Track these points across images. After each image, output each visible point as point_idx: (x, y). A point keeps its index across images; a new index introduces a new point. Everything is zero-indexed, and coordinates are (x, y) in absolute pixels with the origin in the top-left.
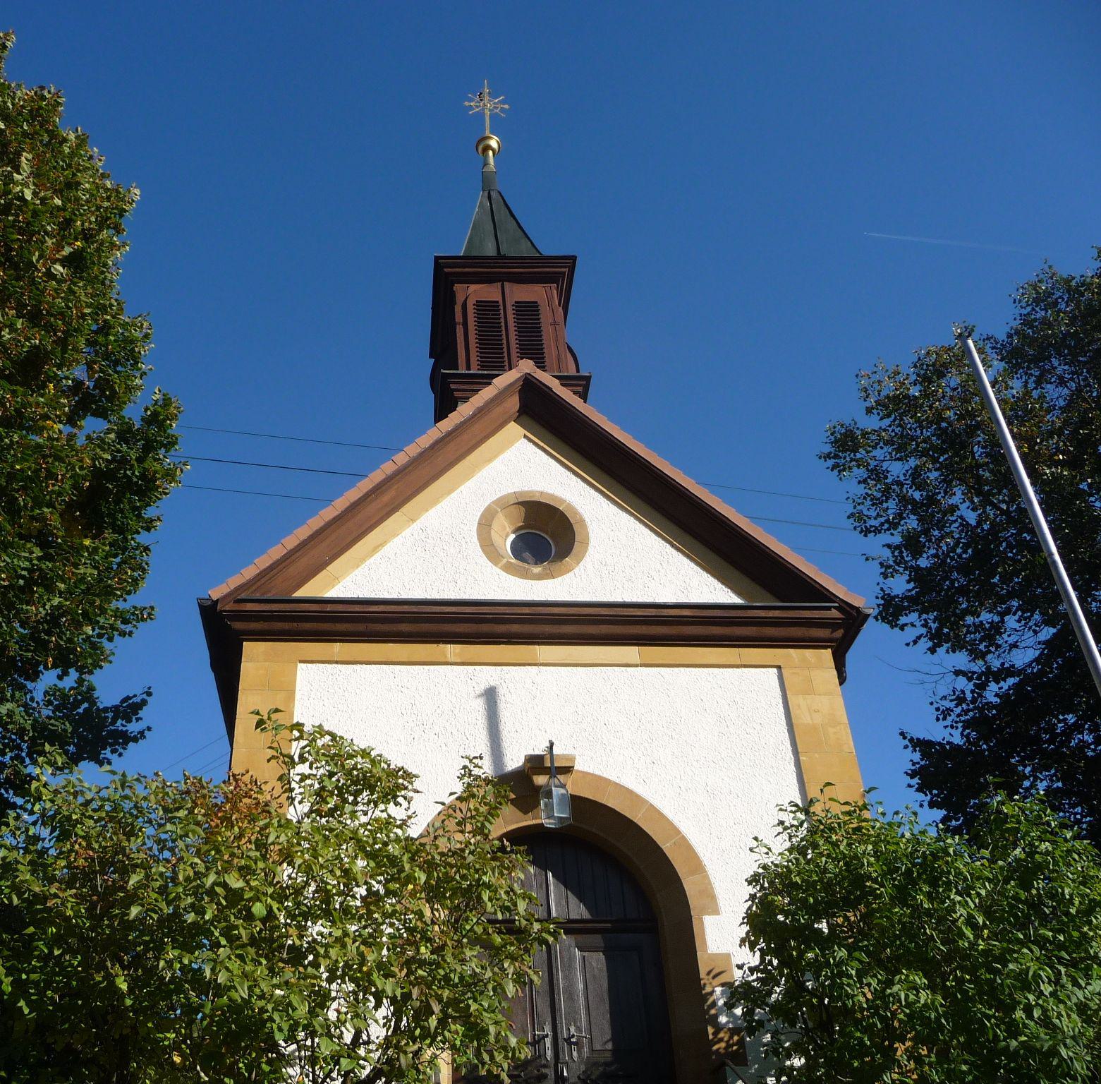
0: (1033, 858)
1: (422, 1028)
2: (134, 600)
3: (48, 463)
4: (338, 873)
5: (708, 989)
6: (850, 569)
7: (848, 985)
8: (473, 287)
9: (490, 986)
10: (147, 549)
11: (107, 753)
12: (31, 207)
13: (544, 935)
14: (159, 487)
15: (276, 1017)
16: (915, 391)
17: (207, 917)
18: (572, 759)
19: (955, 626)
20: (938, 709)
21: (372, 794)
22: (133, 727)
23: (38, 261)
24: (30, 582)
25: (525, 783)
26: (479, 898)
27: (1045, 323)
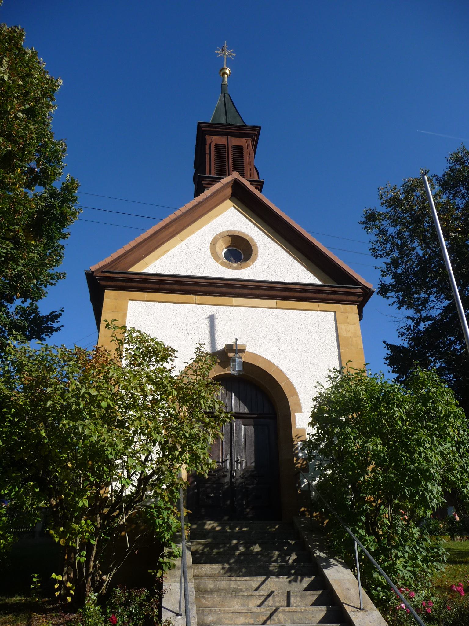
0: (428, 394)
1: (172, 455)
2: (57, 270)
3: (15, 205)
4: (139, 390)
5: (295, 443)
6: (368, 272)
7: (350, 442)
8: (214, 137)
9: (202, 439)
10: (63, 247)
11: (44, 336)
12: (7, 84)
13: (226, 419)
14: (68, 219)
15: (109, 448)
16: (402, 197)
17: (81, 407)
18: (245, 346)
19: (409, 298)
20: (399, 333)
21: (156, 358)
22: (56, 325)
23: (10, 110)
24: (7, 259)
25: (223, 356)
26: (200, 403)
27: (460, 171)
